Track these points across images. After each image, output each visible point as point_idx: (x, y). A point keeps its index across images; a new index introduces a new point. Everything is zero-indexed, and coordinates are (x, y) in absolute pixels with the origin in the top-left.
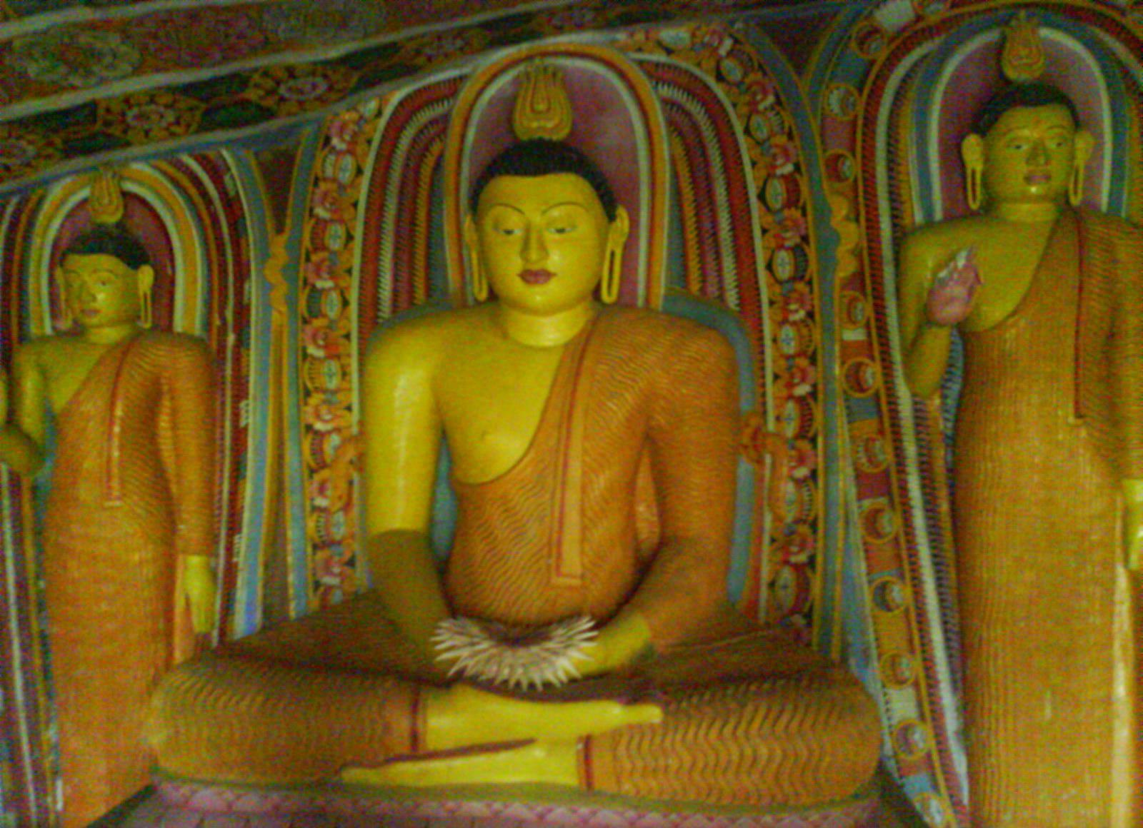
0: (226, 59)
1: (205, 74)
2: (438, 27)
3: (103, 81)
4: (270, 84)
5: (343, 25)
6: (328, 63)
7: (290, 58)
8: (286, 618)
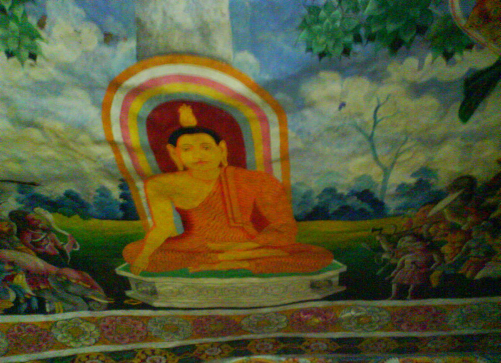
0: (129, 342)
1: (120, 348)
2: (212, 340)
3: (83, 346)
4: (143, 357)
5: (176, 332)
6: (167, 350)
7: (153, 345)
8: (345, 291)
